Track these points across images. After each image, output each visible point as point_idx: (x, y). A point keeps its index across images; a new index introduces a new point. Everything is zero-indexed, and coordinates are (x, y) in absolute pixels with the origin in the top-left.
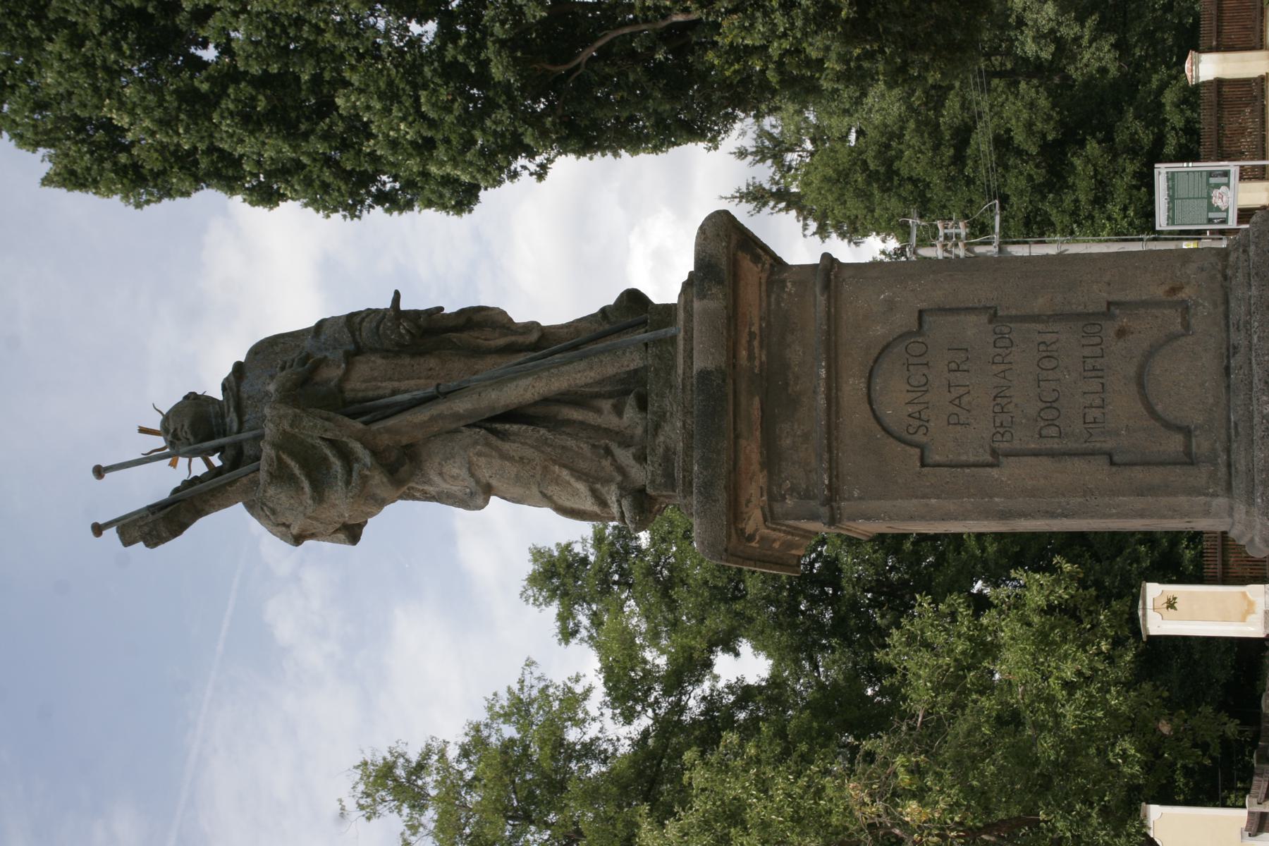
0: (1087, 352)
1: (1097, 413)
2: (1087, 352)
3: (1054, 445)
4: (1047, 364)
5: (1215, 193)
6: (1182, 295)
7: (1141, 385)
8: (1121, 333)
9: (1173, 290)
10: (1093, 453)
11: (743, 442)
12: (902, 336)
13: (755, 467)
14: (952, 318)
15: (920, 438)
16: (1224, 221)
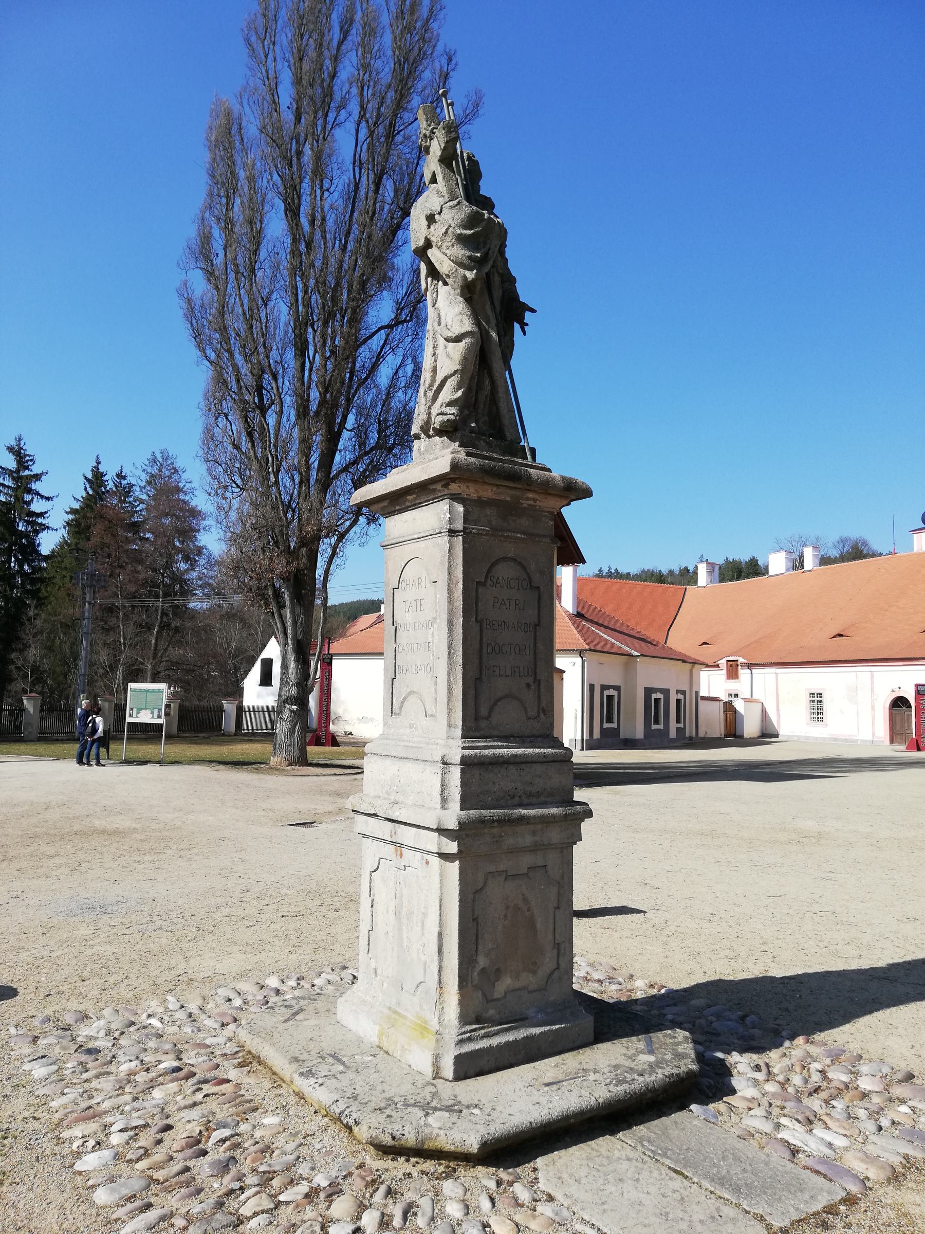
0: (522, 669)
1: (497, 673)
2: (522, 669)
3: (485, 651)
4: (517, 648)
5: (148, 712)
6: (542, 716)
7: (506, 697)
8: (528, 685)
9: (544, 711)
10: (481, 670)
11: (495, 489)
12: (530, 578)
13: (481, 494)
14: (536, 603)
15: (489, 582)
16: (131, 716)
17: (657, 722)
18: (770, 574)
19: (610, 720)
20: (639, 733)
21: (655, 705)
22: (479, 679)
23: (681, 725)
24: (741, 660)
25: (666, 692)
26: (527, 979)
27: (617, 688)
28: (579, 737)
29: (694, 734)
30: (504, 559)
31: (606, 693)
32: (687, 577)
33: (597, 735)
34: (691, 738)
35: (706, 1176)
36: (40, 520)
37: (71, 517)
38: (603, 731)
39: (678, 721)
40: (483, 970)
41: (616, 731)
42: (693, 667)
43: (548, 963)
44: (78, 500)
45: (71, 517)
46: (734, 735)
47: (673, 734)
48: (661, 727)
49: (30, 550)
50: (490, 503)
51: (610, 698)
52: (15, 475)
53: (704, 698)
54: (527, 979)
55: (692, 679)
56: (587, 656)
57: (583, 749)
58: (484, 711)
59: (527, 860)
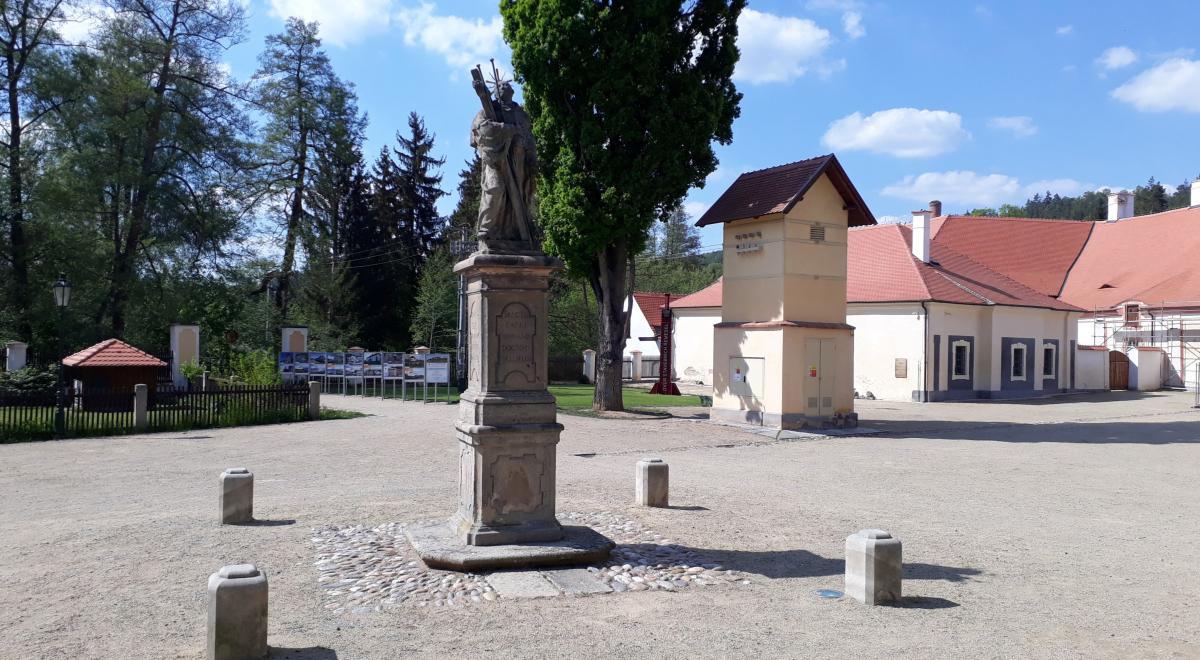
17: (1018, 372)
18: (1109, 219)
19: (960, 371)
20: (996, 384)
21: (1015, 358)
22: (498, 364)
23: (1052, 377)
24: (1142, 305)
25: (1030, 343)
26: (522, 507)
27: (970, 339)
28: (922, 389)
29: (1068, 386)
30: (514, 303)
31: (955, 344)
32: (1095, 207)
33: (943, 386)
34: (1065, 391)
35: (559, 583)
36: (436, 186)
37: (463, 179)
38: (950, 382)
39: (1047, 370)
40: (496, 500)
41: (969, 384)
42: (1068, 315)
43: (535, 501)
44: (469, 164)
45: (463, 179)
46: (1126, 387)
47: (1038, 385)
48: (1023, 378)
49: (428, 214)
50: (503, 276)
51: (960, 350)
52: (413, 146)
53: (1082, 348)
54: (522, 507)
55: (1070, 330)
56: (932, 307)
57: (926, 401)
58: (501, 379)
59: (521, 452)
